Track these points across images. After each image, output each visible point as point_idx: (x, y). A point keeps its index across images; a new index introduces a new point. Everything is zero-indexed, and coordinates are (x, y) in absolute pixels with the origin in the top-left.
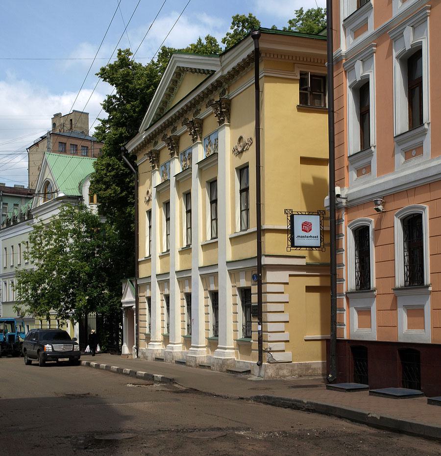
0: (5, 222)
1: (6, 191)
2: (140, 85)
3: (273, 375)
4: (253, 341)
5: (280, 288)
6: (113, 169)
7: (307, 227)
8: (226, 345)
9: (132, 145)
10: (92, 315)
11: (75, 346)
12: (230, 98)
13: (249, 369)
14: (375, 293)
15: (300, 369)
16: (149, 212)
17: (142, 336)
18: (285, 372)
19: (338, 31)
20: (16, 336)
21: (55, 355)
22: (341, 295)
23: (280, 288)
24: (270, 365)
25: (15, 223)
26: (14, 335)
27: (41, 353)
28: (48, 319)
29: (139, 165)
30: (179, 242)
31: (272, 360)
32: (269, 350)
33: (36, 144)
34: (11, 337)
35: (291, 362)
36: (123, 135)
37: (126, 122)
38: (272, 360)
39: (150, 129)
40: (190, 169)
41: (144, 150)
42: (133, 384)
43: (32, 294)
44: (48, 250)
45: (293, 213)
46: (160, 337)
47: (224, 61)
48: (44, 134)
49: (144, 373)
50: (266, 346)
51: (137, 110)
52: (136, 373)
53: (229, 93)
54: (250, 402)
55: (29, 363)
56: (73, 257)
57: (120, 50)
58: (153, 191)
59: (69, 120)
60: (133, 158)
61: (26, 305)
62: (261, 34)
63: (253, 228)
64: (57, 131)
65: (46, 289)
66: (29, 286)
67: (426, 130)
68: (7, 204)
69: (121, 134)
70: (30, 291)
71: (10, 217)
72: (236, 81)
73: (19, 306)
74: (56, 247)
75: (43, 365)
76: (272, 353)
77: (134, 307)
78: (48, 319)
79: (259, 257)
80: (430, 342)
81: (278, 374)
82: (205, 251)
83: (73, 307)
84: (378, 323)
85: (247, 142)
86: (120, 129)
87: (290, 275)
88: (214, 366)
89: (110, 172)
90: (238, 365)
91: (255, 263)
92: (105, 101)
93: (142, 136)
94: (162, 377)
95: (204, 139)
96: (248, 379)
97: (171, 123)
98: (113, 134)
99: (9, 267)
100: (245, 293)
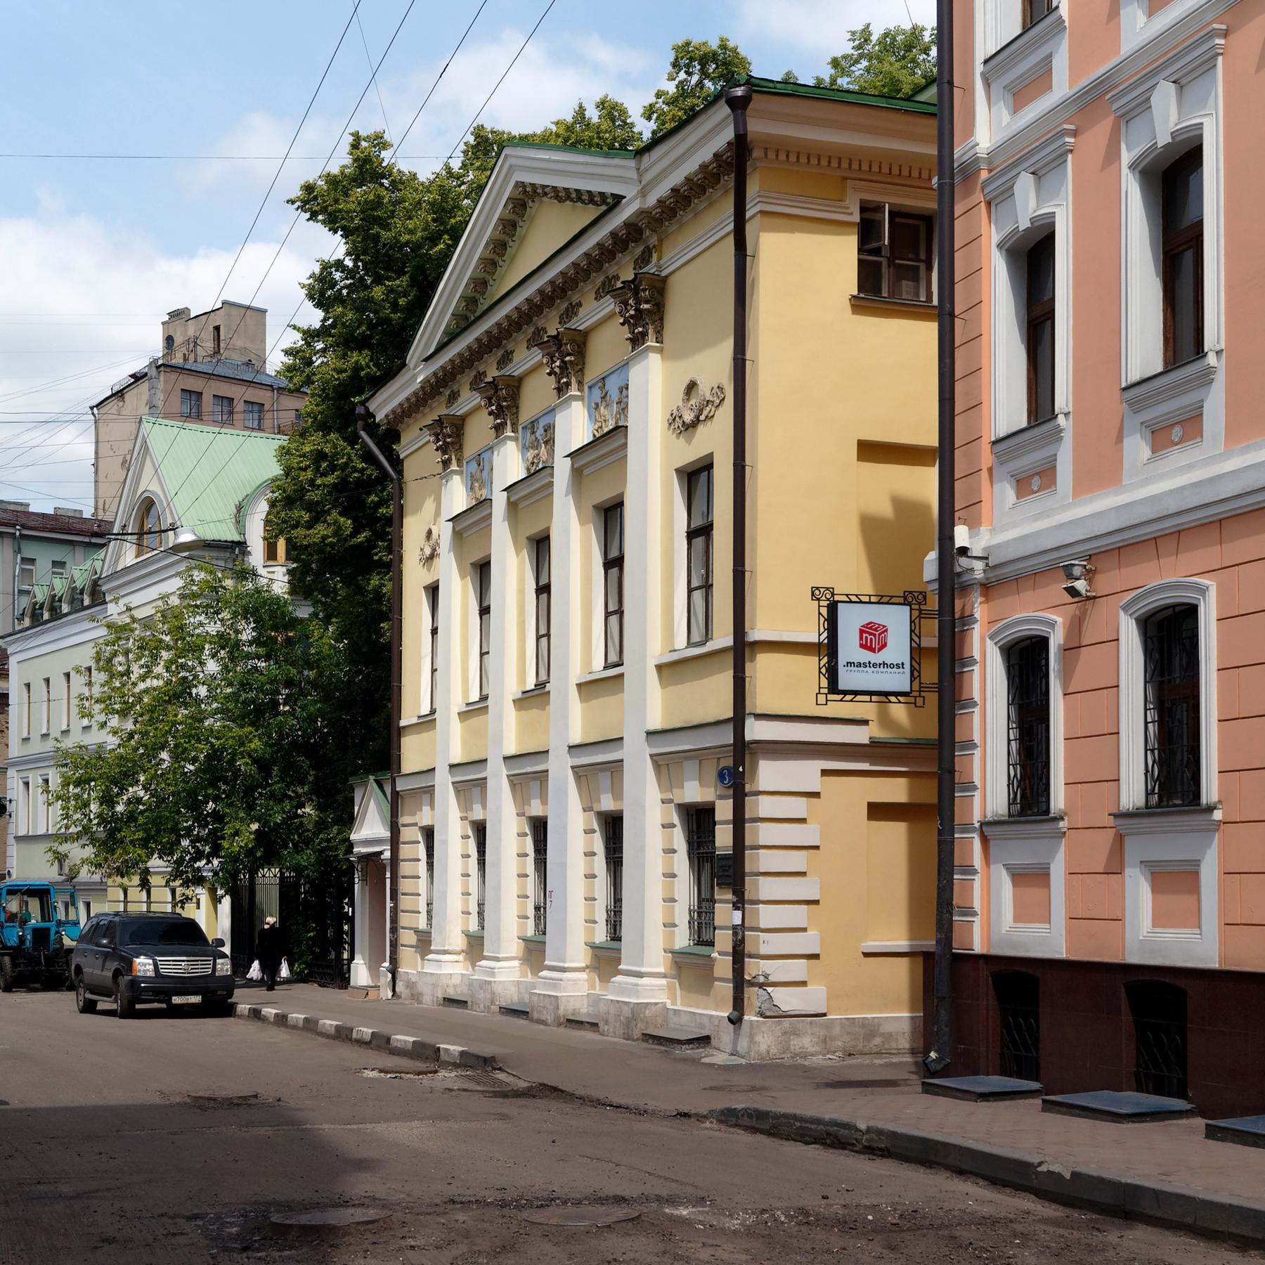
1: (32, 524)
3: (773, 1051)
5: (797, 807)
6: (333, 468)
7: (873, 637)
9: (380, 406)
10: (269, 876)
11: (219, 961)
12: (664, 274)
13: (705, 1033)
14: (1061, 824)
15: (849, 1033)
16: (433, 591)
17: (407, 937)
19: (969, 92)
21: (163, 988)
23: (797, 807)
24: (764, 1023)
25: (56, 615)
26: (48, 930)
27: (124, 980)
32: (762, 979)
33: (119, 394)
34: (41, 935)
35: (825, 1015)
36: (363, 373)
40: (548, 471)
42: (381, 1071)
43: (99, 816)
44: (146, 691)
45: (836, 598)
46: (459, 942)
47: (646, 170)
48: (139, 365)
49: (411, 1039)
50: (753, 968)
51: (402, 301)
52: (388, 1040)
53: (660, 259)
54: (707, 1124)
56: (217, 711)
58: (444, 532)
60: (389, 436)
61: (83, 846)
62: (754, 96)
63: (723, 638)
64: (178, 360)
66: (93, 794)
67: (1210, 371)
68: (32, 561)
69: (357, 368)
70: (94, 807)
71: (40, 598)
73: (63, 848)
74: (168, 683)
75: (129, 1012)
76: (770, 990)
77: (387, 855)
78: (145, 884)
80: (1215, 965)
81: (786, 1049)
85: (709, 397)
86: (355, 357)
87: (825, 773)
88: (607, 1022)
89: (323, 475)
90: (674, 1020)
91: (727, 737)
92: (312, 276)
94: (462, 1053)
95: (590, 388)
97: (495, 342)
98: (334, 370)
99: (35, 737)
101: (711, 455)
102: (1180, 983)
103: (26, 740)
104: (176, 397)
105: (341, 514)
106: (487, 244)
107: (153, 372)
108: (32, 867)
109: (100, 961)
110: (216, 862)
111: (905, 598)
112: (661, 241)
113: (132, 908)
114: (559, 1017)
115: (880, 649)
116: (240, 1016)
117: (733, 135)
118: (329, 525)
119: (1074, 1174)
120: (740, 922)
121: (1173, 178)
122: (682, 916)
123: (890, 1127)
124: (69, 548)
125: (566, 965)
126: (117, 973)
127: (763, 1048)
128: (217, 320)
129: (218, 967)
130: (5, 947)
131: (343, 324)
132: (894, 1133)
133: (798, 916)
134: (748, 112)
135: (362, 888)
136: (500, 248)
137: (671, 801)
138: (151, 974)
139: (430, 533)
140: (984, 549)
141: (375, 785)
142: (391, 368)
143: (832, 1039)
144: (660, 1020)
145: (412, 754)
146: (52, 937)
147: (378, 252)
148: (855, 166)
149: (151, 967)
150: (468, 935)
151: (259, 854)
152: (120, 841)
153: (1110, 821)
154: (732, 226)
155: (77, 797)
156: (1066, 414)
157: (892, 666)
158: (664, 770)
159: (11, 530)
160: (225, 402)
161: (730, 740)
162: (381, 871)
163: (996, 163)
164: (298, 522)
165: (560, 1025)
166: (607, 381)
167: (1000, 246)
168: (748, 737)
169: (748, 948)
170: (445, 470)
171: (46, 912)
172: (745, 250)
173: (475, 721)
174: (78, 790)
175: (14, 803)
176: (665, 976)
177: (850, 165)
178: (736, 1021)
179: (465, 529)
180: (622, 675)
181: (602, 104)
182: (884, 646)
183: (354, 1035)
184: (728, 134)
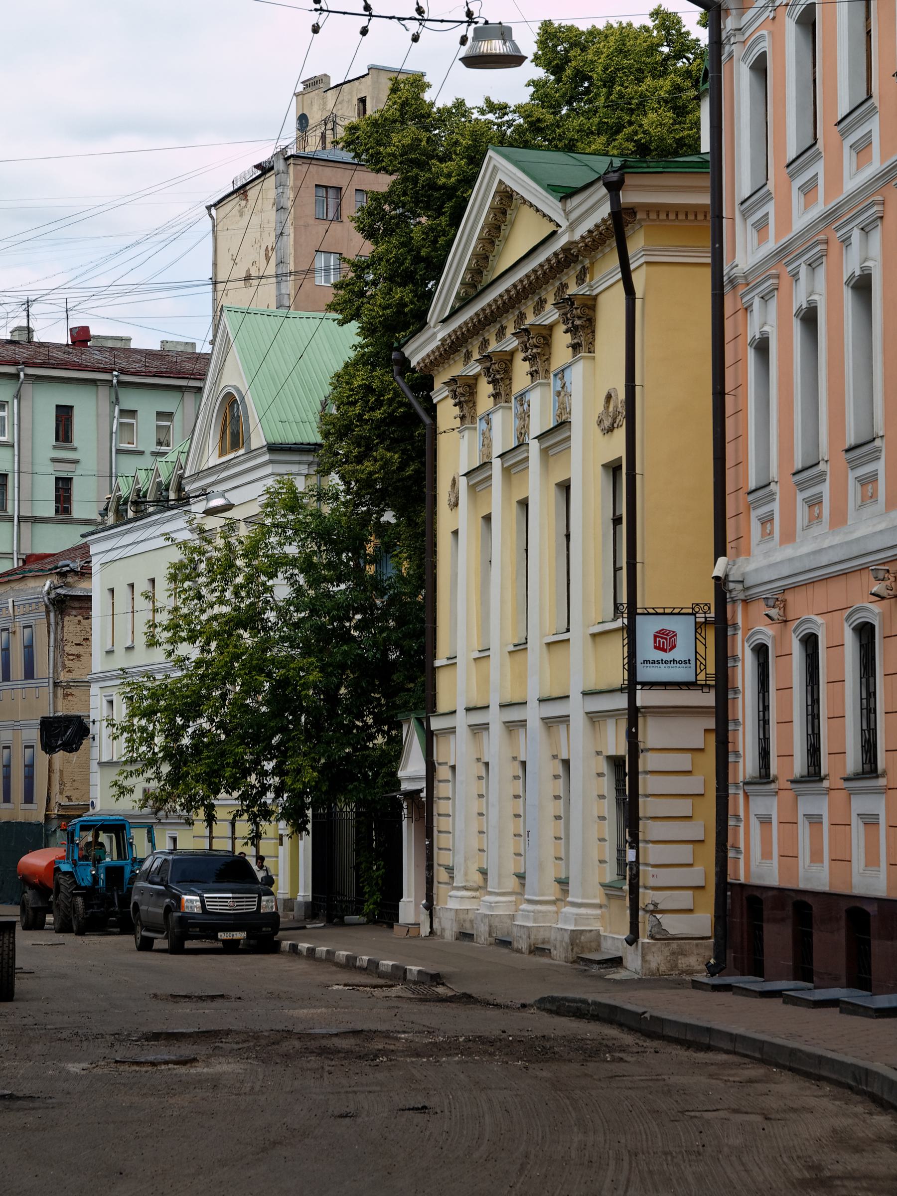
0: (112, 506)
3: (663, 968)
6: (379, 404)
7: (665, 641)
10: (346, 809)
11: (263, 898)
12: (595, 293)
13: (619, 954)
20: (128, 870)
21: (208, 925)
22: (736, 784)
24: (654, 945)
25: (141, 515)
26: (121, 869)
28: (210, 819)
31: (658, 933)
33: (241, 191)
36: (406, 310)
38: (658, 933)
43: (164, 749)
44: (215, 618)
48: (264, 155)
49: (391, 963)
50: (646, 897)
53: (592, 279)
54: (532, 1011)
55: (146, 945)
59: (355, 102)
60: (423, 383)
65: (202, 733)
66: (156, 726)
67: (773, 494)
68: (132, 413)
70: (159, 740)
71: (124, 492)
75: (177, 949)
76: (658, 916)
78: (210, 819)
80: (826, 888)
81: (674, 967)
86: (398, 293)
89: (372, 409)
91: (621, 701)
92: (362, 209)
94: (419, 972)
95: (555, 375)
96: (607, 977)
97: (490, 319)
99: (119, 649)
102: (806, 899)
104: (309, 196)
106: (483, 228)
107: (280, 165)
111: (693, 609)
112: (592, 264)
113: (218, 845)
115: (670, 650)
117: (609, 210)
118: (376, 460)
120: (634, 860)
124: (178, 395)
126: (168, 910)
127: (653, 966)
128: (364, 89)
129: (263, 903)
130: (79, 887)
135: (409, 826)
137: (598, 753)
145: (454, 689)
149: (199, 904)
151: (324, 789)
152: (194, 774)
153: (789, 785)
154: (620, 276)
155: (143, 729)
159: (106, 377)
161: (625, 704)
162: (424, 807)
166: (567, 373)
170: (462, 425)
171: (123, 846)
172: (634, 294)
173: (519, 657)
174: (143, 722)
175: (97, 724)
176: (600, 906)
180: (568, 640)
182: (674, 647)
184: (605, 210)
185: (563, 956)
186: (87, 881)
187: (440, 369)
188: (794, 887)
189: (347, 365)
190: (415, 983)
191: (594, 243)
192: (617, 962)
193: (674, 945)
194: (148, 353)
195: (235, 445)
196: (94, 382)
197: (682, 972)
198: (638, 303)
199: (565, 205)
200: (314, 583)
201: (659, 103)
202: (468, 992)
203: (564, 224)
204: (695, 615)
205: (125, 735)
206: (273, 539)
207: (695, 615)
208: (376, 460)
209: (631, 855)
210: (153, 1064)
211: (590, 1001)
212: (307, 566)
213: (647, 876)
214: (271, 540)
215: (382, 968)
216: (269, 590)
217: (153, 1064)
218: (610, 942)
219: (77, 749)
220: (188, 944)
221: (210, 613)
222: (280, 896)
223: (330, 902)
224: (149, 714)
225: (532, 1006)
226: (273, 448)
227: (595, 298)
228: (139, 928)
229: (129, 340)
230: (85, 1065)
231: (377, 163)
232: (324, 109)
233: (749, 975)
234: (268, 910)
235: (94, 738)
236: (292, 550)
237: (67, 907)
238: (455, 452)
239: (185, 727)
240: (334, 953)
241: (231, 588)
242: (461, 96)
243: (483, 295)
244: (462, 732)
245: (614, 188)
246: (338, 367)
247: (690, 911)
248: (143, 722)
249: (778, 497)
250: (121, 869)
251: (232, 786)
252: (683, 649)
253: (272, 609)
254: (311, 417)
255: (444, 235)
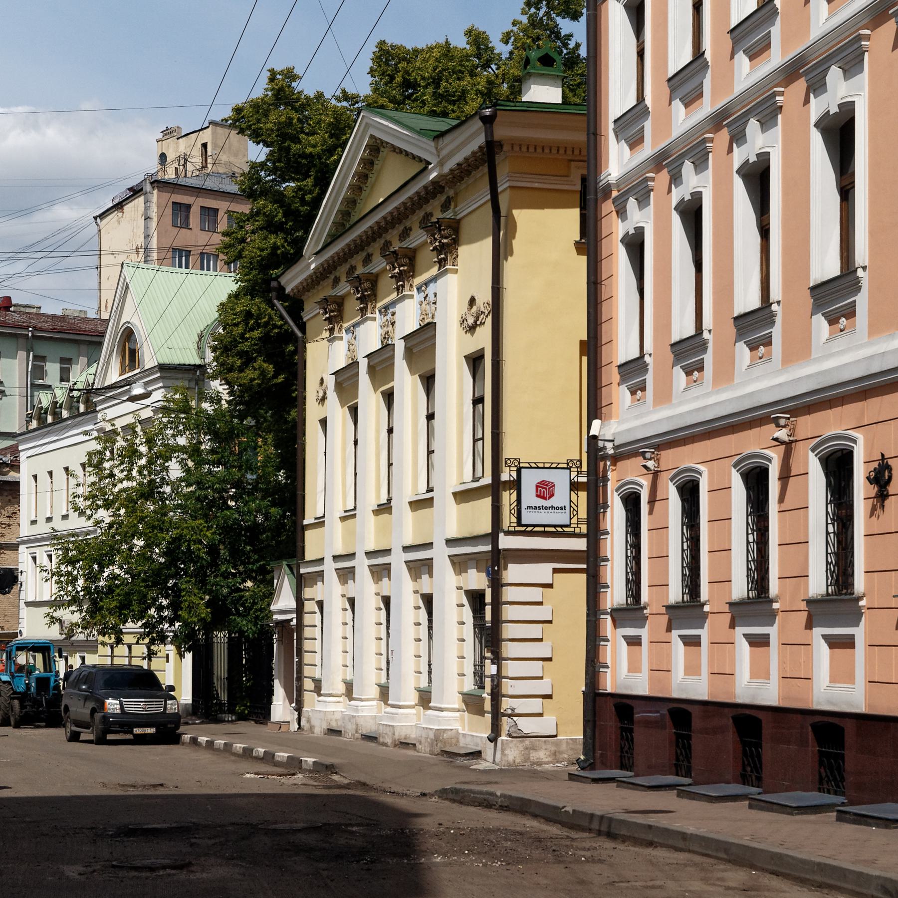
1: (42, 326)
2: (314, 146)
3: (518, 760)
4: (488, 700)
5: (535, 594)
6: (258, 326)
7: (545, 490)
8: (399, 701)
9: (291, 280)
10: (221, 637)
11: (169, 702)
12: (458, 217)
13: (479, 749)
14: (645, 611)
15: (572, 749)
16: (324, 422)
17: (308, 684)
18: (542, 755)
19: (607, 138)
21: (126, 722)
23: (535, 594)
26: (48, 679)
27: (98, 716)
29: (308, 320)
30: (372, 497)
32: (509, 712)
34: (43, 683)
35: (556, 736)
36: (279, 252)
37: (286, 223)
39: (323, 252)
40: (391, 347)
41: (315, 291)
42: (256, 774)
45: (522, 465)
46: (375, 692)
47: (442, 149)
49: (286, 755)
50: (506, 704)
51: (308, 197)
52: (274, 755)
53: (456, 206)
54: (433, 799)
55: (74, 737)
56: (178, 506)
57: (273, 73)
58: (330, 381)
59: (200, 146)
60: (295, 307)
61: (73, 612)
62: (498, 112)
63: (487, 480)
64: (170, 175)
65: (115, 577)
69: (275, 247)
70: (81, 582)
72: (476, 180)
73: (58, 614)
74: (141, 484)
75: (101, 740)
76: (515, 718)
77: (294, 622)
79: (493, 537)
80: (705, 698)
81: (527, 759)
82: (416, 511)
83: (177, 618)
84: (650, 663)
85: (482, 309)
86: (272, 239)
87: (555, 571)
88: (420, 743)
89: (252, 330)
90: (462, 742)
93: (310, 264)
98: (258, 248)
99: (41, 520)
100: (476, 599)
101: (483, 349)
103: (34, 522)
105: (264, 361)
107: (148, 187)
108: (34, 626)
109: (82, 702)
110: (177, 624)
111: (568, 464)
112: (456, 194)
113: (117, 661)
114: (395, 741)
115: (549, 498)
116: (183, 744)
119: (574, 811)
120: (495, 673)
121: (840, 133)
122: (469, 670)
123: (521, 796)
125: (401, 704)
126: (93, 711)
130: (15, 693)
131: (264, 213)
132: (510, 796)
133: (535, 668)
134: (494, 125)
136: (363, 178)
137: (461, 588)
138: (118, 711)
139: (322, 381)
140: (614, 434)
141: (287, 569)
142: (294, 257)
143: (561, 753)
144: (454, 741)
145: (315, 545)
146: (52, 684)
147: (289, 159)
148: (577, 152)
150: (419, 691)
152: (106, 608)
154: (489, 197)
155: (69, 573)
156: (650, 355)
157: (557, 508)
158: (457, 566)
160: (211, 213)
162: (292, 633)
163: (621, 187)
164: (232, 366)
165: (395, 746)
167: (816, 125)
168: (501, 546)
169: (504, 691)
174: (70, 568)
177: (573, 151)
178: (493, 739)
179: (345, 380)
180: (432, 498)
181: (469, 33)
182: (553, 495)
183: (254, 754)
184: (481, 140)
185: (428, 750)
186: (21, 688)
187: (310, 294)
188: (668, 696)
189: (230, 296)
190: (310, 771)
191: (463, 172)
192: (477, 754)
193: (528, 741)
194: (54, 317)
195: (132, 367)
196: (15, 336)
197: (533, 764)
198: (503, 220)
199: (437, 144)
200: (199, 464)
201: (477, 95)
202: (362, 780)
203: (434, 161)
204: (569, 469)
205: (55, 578)
206: (169, 432)
207: (569, 469)
208: (255, 369)
209: (491, 669)
210: (151, 869)
211: (498, 794)
212: (194, 451)
213: (508, 687)
214: (167, 432)
215: (277, 759)
216: (167, 469)
217: (151, 869)
218: (468, 739)
219: (9, 592)
220: (110, 737)
221: (120, 486)
222: (182, 702)
223: (206, 706)
224: (72, 562)
225: (433, 795)
226: (162, 367)
227: (458, 222)
228: (68, 725)
229: (40, 308)
230: (81, 869)
231: (257, 137)
232: (177, 151)
233: (616, 769)
234: (173, 711)
235: (21, 584)
236: (182, 441)
237: (6, 708)
238: (324, 357)
239: (101, 571)
240: (232, 745)
241: (136, 469)
242: (321, 90)
243: (354, 229)
244: (331, 576)
245: (488, 121)
246: (224, 298)
247: (541, 715)
248: (70, 568)
249: (710, 346)
250: (48, 679)
251: (136, 619)
252: (562, 495)
253: (168, 484)
254: (191, 346)
255: (309, 193)
